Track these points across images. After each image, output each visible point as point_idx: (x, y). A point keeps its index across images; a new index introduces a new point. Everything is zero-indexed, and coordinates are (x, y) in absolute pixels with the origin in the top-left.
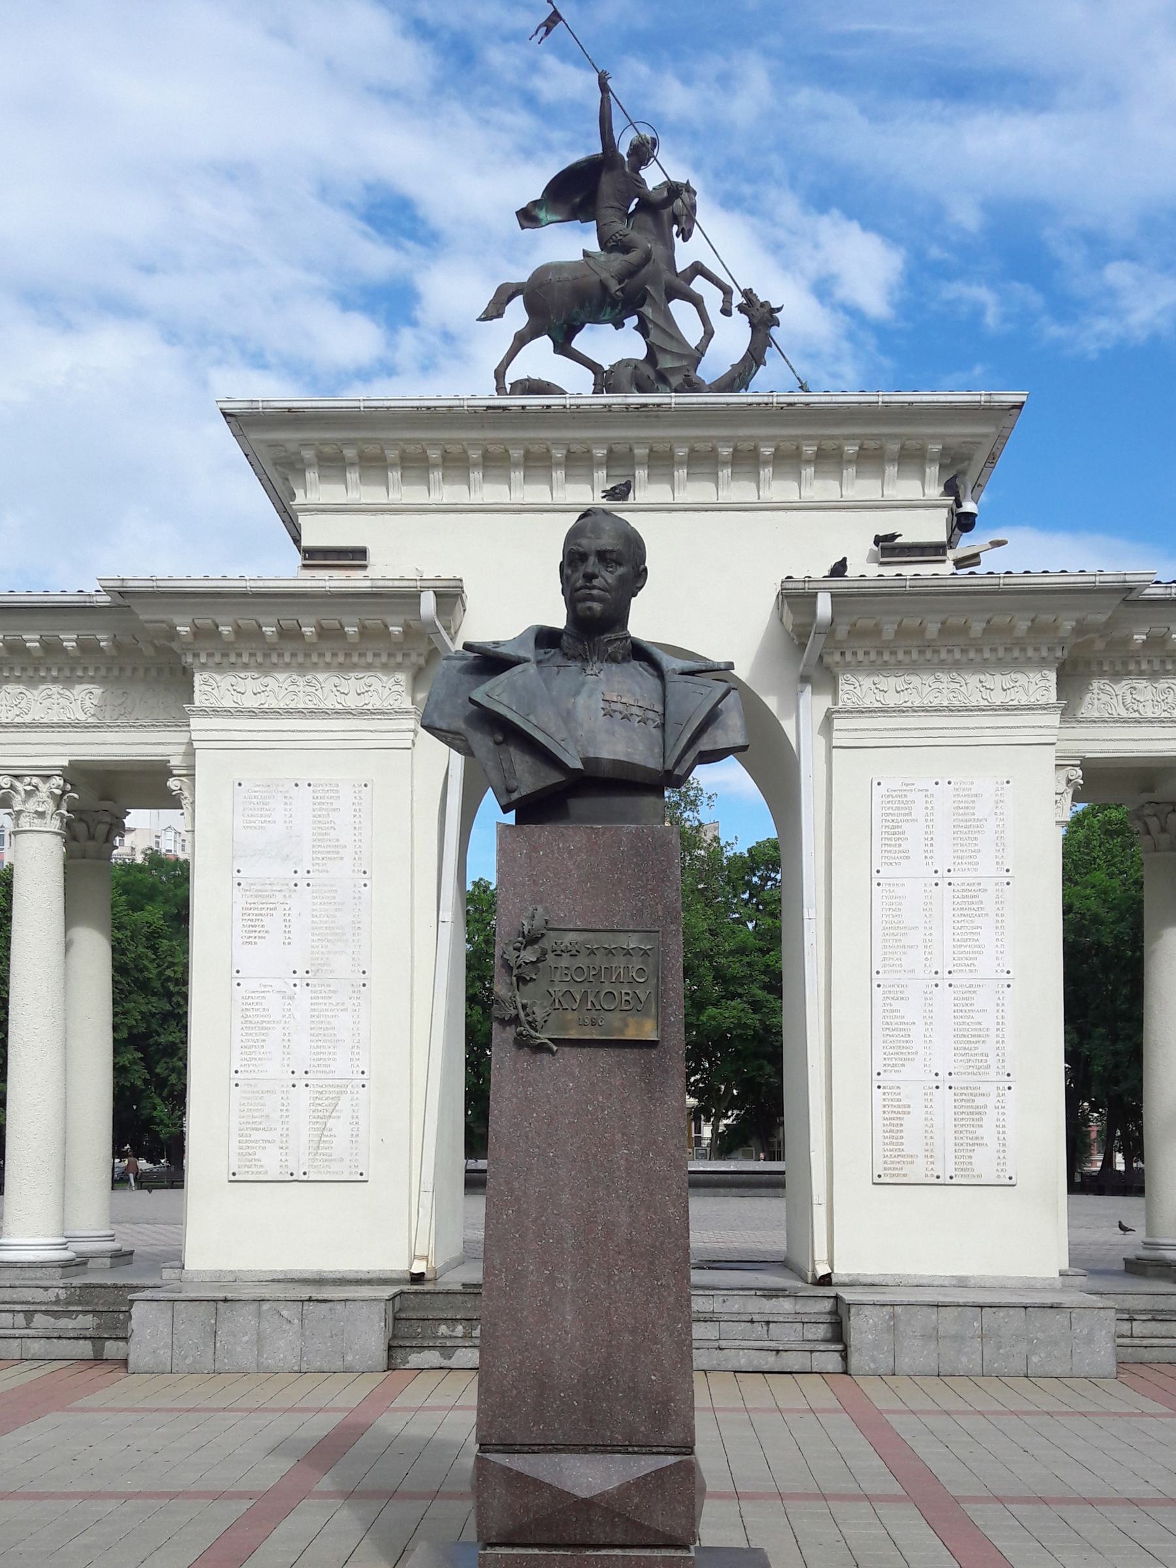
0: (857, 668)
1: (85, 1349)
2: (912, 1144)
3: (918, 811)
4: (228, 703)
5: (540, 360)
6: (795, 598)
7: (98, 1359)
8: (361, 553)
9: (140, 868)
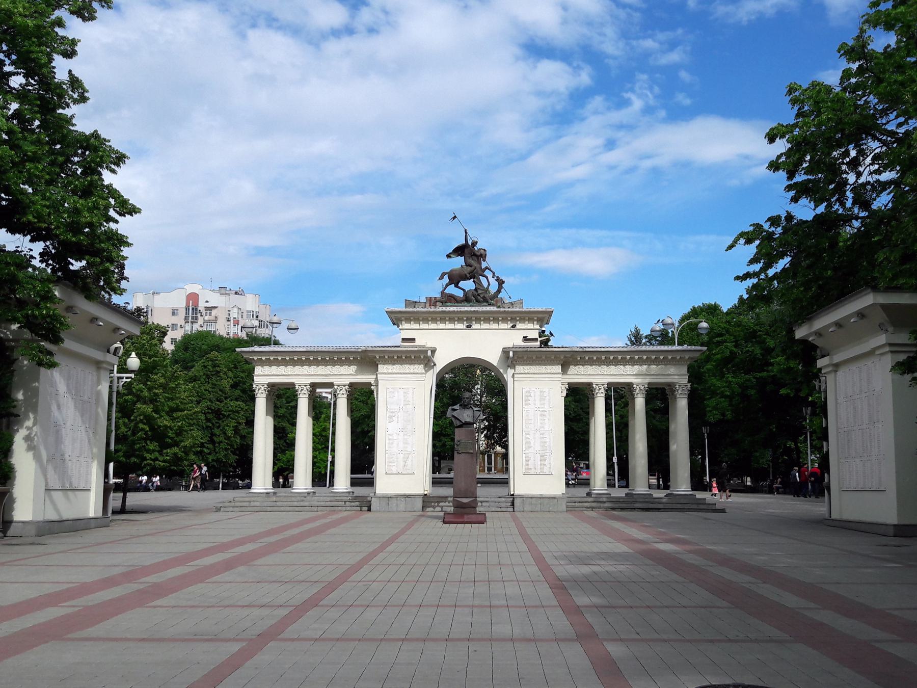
0: (519, 365)
1: (359, 508)
5: (452, 290)
6: (505, 352)
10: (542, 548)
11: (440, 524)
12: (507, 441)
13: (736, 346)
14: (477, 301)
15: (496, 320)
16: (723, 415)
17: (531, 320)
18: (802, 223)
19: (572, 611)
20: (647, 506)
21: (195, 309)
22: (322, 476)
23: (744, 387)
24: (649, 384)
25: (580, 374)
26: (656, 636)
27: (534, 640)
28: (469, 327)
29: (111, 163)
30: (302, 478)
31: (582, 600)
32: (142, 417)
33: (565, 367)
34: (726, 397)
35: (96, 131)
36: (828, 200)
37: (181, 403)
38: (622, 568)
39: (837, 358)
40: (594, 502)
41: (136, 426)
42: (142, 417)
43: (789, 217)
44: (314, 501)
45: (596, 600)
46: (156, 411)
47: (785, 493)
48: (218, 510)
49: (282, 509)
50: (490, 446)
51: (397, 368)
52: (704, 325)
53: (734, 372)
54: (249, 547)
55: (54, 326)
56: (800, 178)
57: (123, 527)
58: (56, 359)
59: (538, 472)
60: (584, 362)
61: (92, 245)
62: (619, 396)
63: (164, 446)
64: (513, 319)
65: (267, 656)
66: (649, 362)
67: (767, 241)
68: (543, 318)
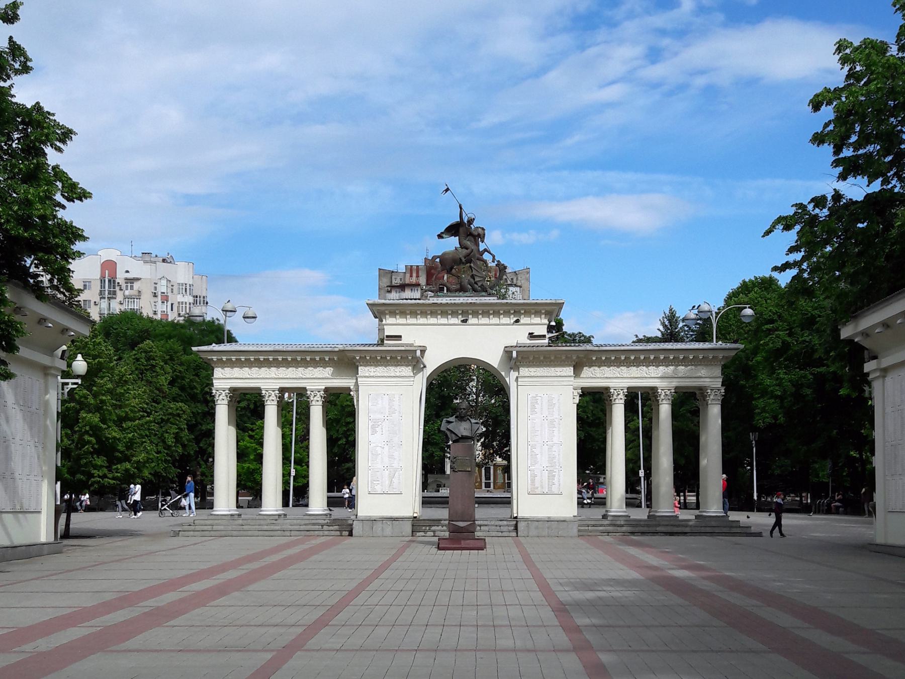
1: (338, 533)
2: (537, 484)
3: (539, 402)
6: (508, 352)
7: (341, 536)
8: (400, 337)
9: (182, 326)
10: (547, 575)
11: (434, 550)
12: (509, 450)
13: (790, 335)
14: (475, 290)
15: (497, 314)
16: (775, 418)
17: (538, 313)
18: (852, 202)
19: (572, 629)
20: (671, 529)
21: (112, 281)
22: (296, 493)
23: (797, 385)
24: (676, 388)
26: (646, 648)
27: (535, 651)
28: (464, 321)
29: (57, 140)
31: (582, 621)
32: (87, 428)
33: (578, 368)
34: (777, 397)
35: (38, 103)
36: (883, 174)
37: (132, 411)
38: (627, 593)
39: (886, 362)
40: (609, 525)
41: (81, 438)
42: (87, 428)
43: (837, 196)
44: (286, 524)
45: (595, 621)
46: (103, 421)
47: (846, 513)
48: (176, 534)
49: (250, 533)
50: (489, 457)
51: (380, 370)
52: (748, 311)
53: (786, 367)
54: (232, 574)
55: (9, 333)
56: (847, 153)
57: (77, 554)
58: (12, 368)
59: (546, 491)
60: (600, 363)
61: (45, 239)
62: (640, 402)
63: (112, 461)
64: (517, 313)
65: (297, 661)
66: (676, 362)
67: (812, 226)
68: (552, 310)
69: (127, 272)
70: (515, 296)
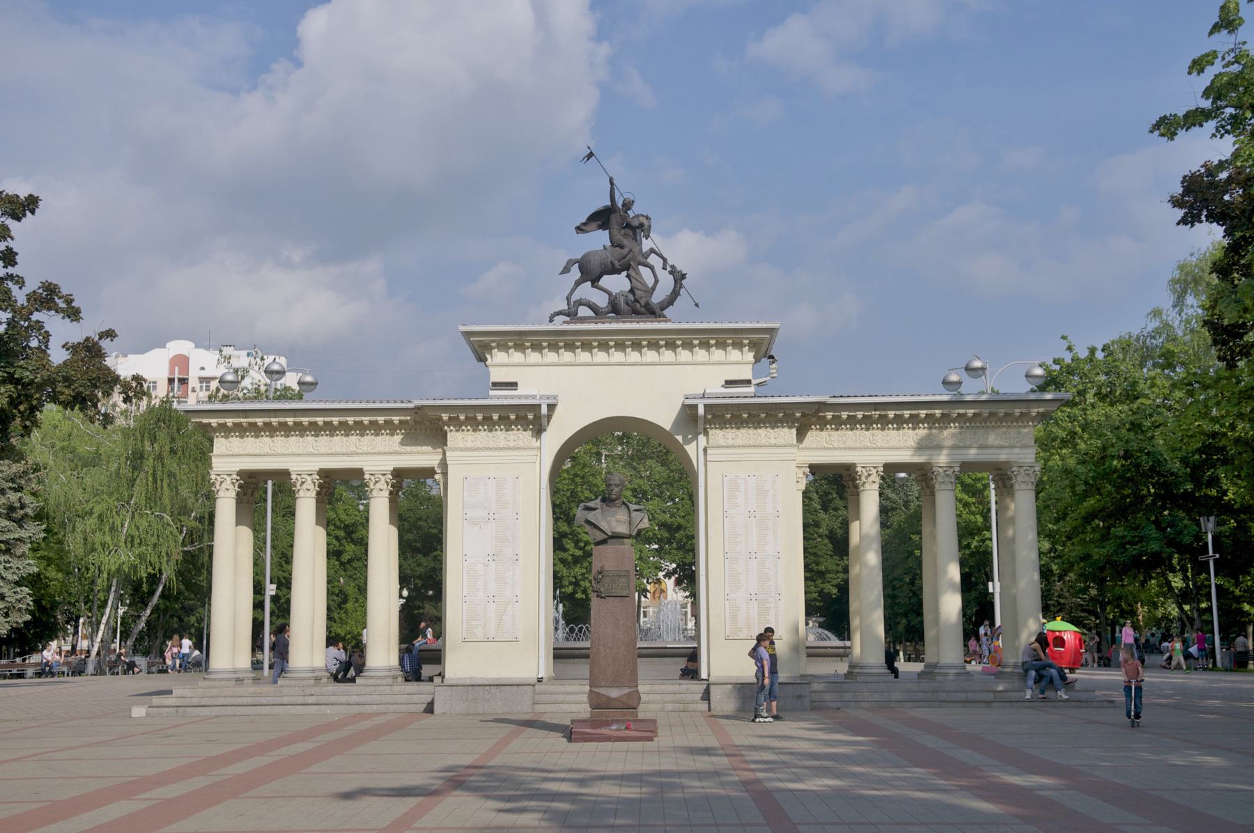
4: (461, 445)
5: (586, 291)
25: (829, 447)
30: (309, 645)
51: (482, 437)
69: (203, 368)
70: (676, 319)
